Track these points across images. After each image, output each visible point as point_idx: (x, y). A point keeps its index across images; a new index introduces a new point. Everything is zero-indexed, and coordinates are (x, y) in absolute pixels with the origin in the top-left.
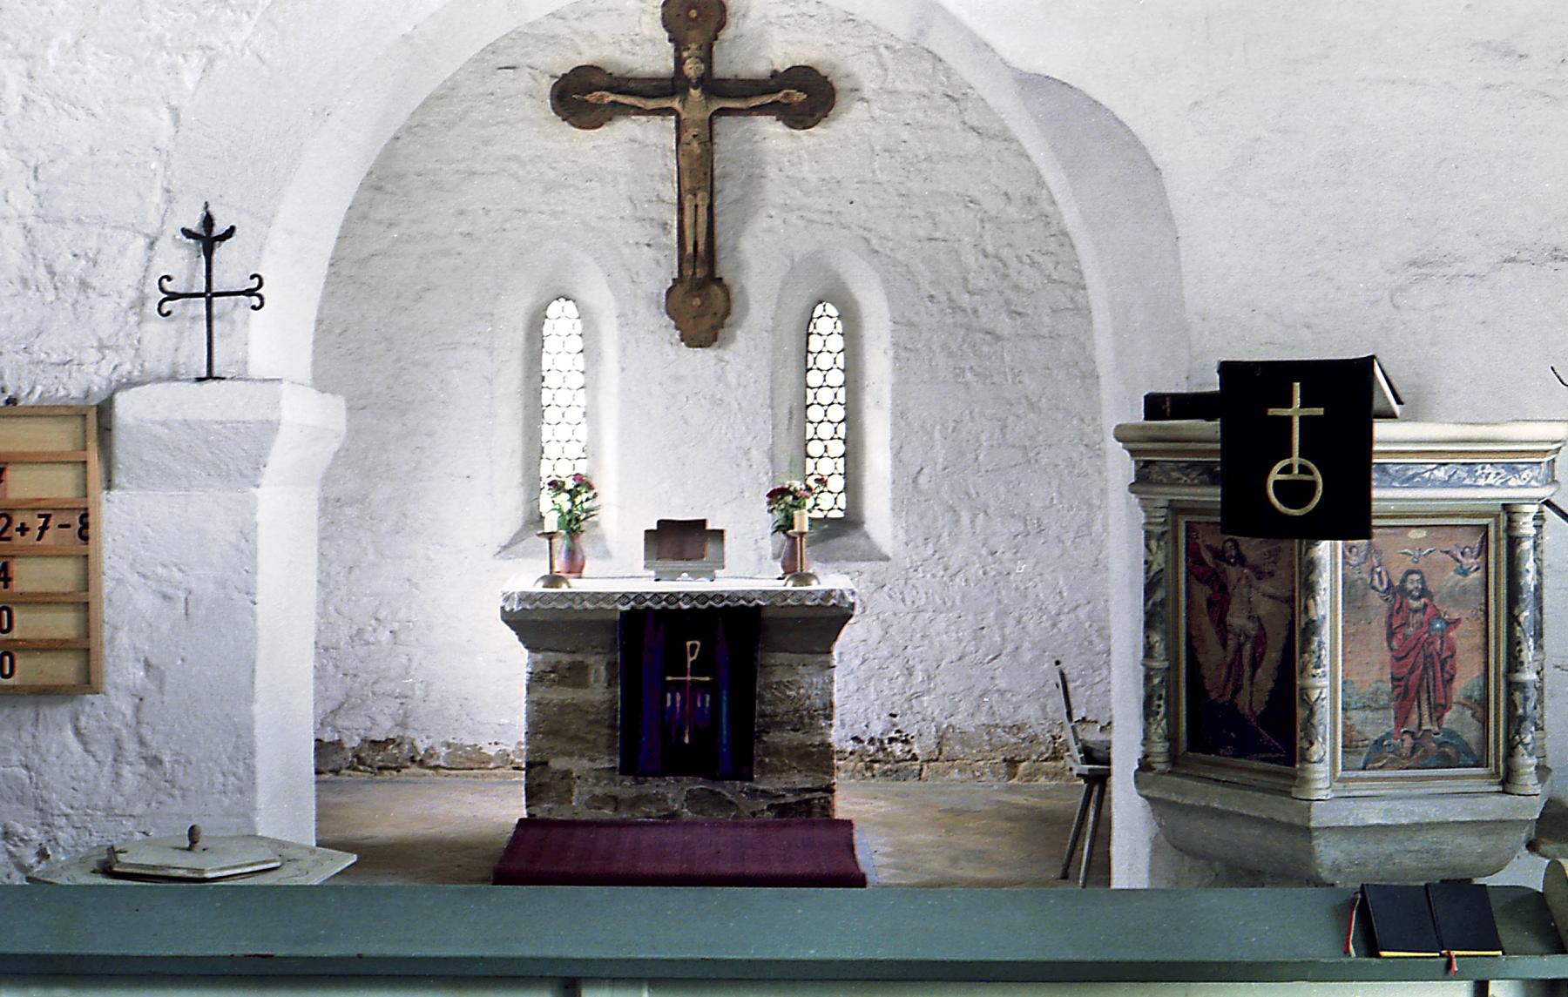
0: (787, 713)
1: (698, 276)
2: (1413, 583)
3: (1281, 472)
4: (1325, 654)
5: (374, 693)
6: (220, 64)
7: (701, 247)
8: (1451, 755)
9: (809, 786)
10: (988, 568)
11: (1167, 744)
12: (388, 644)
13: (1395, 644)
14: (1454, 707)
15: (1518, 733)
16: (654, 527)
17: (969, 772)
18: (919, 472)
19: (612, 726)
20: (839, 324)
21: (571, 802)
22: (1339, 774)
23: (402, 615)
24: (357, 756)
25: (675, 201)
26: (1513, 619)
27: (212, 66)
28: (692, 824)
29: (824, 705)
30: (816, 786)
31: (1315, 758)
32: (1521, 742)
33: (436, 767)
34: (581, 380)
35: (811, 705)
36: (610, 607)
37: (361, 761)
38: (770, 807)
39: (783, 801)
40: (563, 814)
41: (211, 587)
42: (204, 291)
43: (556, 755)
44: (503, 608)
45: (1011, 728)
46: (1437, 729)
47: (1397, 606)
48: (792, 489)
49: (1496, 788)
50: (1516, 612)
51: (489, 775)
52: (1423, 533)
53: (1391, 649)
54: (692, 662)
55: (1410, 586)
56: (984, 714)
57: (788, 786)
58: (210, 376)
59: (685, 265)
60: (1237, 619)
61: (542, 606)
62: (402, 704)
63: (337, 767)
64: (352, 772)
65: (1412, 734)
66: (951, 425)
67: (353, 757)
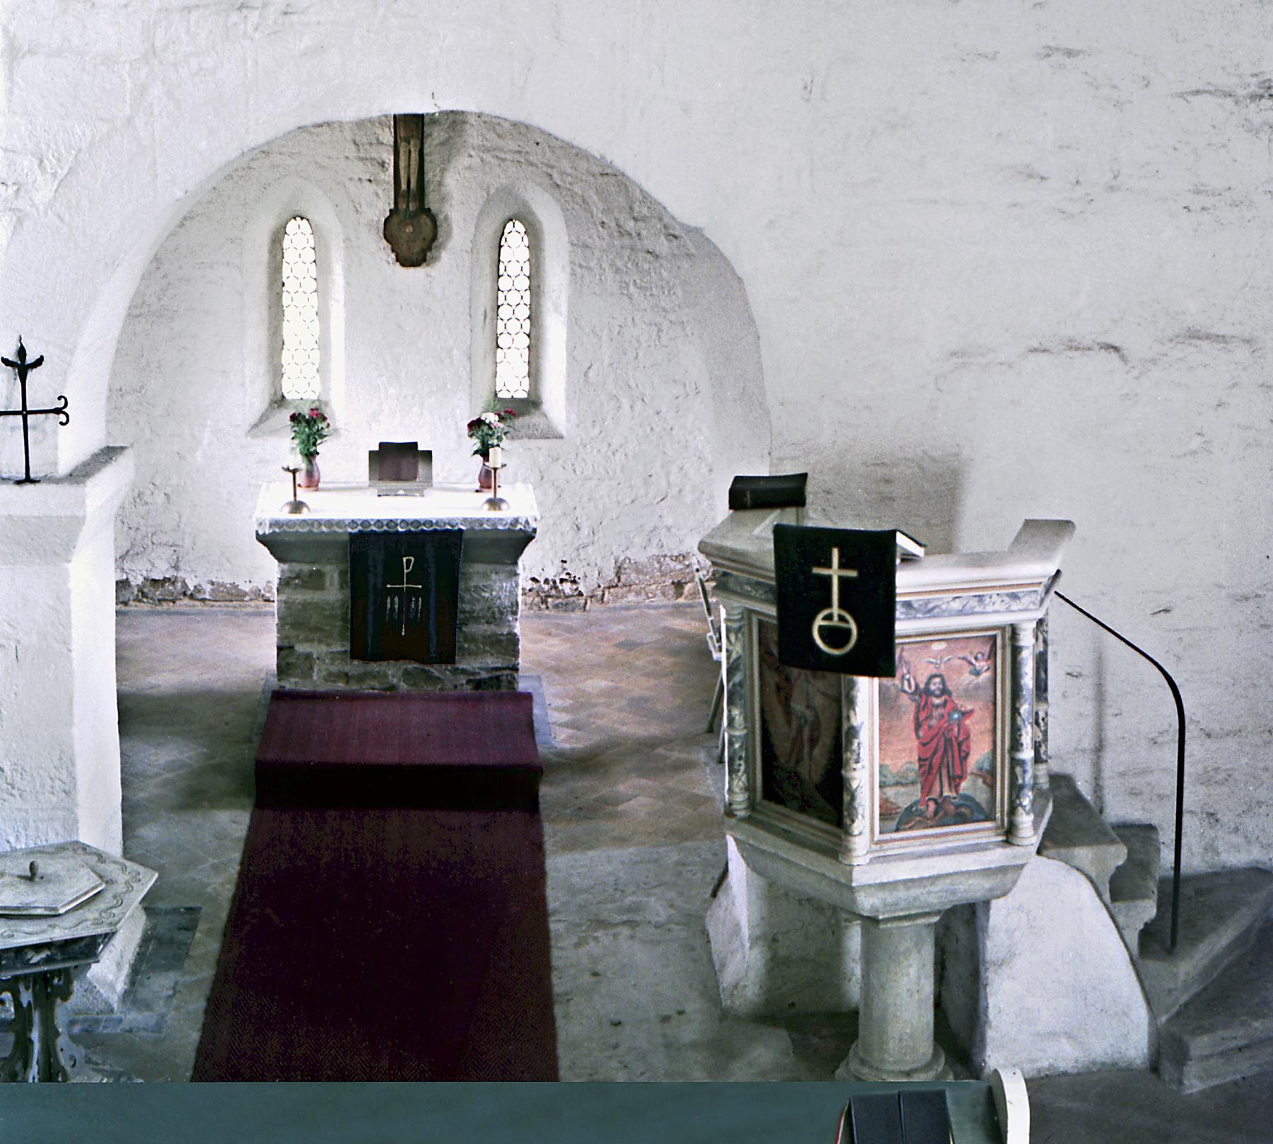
0: (482, 610)
1: (411, 209)
2: (935, 685)
3: (825, 618)
4: (864, 753)
5: (153, 543)
6: (28, 224)
7: (413, 185)
8: (965, 813)
9: (500, 665)
10: (654, 426)
11: (746, 795)
12: (163, 504)
13: (921, 734)
14: (969, 777)
15: (1018, 797)
16: (377, 448)
17: (643, 594)
18: (590, 367)
19: (344, 620)
20: (526, 238)
21: (312, 677)
22: (877, 837)
23: (174, 481)
24: (141, 590)
25: (392, 144)
26: (1015, 711)
27: (21, 224)
28: (406, 698)
29: (512, 603)
30: (505, 666)
31: (856, 832)
32: (1021, 804)
33: (203, 600)
34: (314, 285)
35: (501, 604)
36: (341, 531)
37: (145, 596)
38: (469, 682)
39: (478, 677)
40: (305, 686)
41: (35, 639)
42: (21, 409)
43: (299, 641)
44: (257, 532)
45: (677, 557)
46: (955, 795)
47: (922, 704)
48: (487, 422)
49: (1000, 838)
50: (1018, 705)
51: (245, 607)
52: (943, 645)
53: (918, 737)
54: (407, 573)
55: (933, 687)
56: (655, 545)
57: (484, 665)
58: (28, 480)
59: (400, 200)
60: (798, 706)
61: (288, 530)
62: (175, 551)
63: (126, 600)
64: (138, 604)
65: (935, 801)
66: (617, 329)
67: (138, 591)
